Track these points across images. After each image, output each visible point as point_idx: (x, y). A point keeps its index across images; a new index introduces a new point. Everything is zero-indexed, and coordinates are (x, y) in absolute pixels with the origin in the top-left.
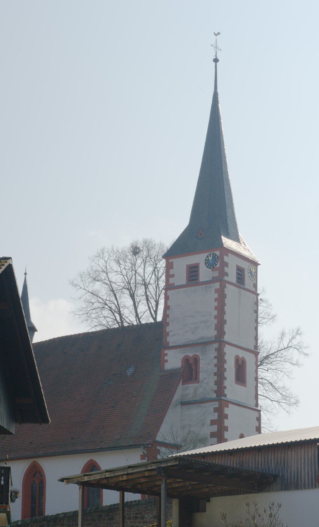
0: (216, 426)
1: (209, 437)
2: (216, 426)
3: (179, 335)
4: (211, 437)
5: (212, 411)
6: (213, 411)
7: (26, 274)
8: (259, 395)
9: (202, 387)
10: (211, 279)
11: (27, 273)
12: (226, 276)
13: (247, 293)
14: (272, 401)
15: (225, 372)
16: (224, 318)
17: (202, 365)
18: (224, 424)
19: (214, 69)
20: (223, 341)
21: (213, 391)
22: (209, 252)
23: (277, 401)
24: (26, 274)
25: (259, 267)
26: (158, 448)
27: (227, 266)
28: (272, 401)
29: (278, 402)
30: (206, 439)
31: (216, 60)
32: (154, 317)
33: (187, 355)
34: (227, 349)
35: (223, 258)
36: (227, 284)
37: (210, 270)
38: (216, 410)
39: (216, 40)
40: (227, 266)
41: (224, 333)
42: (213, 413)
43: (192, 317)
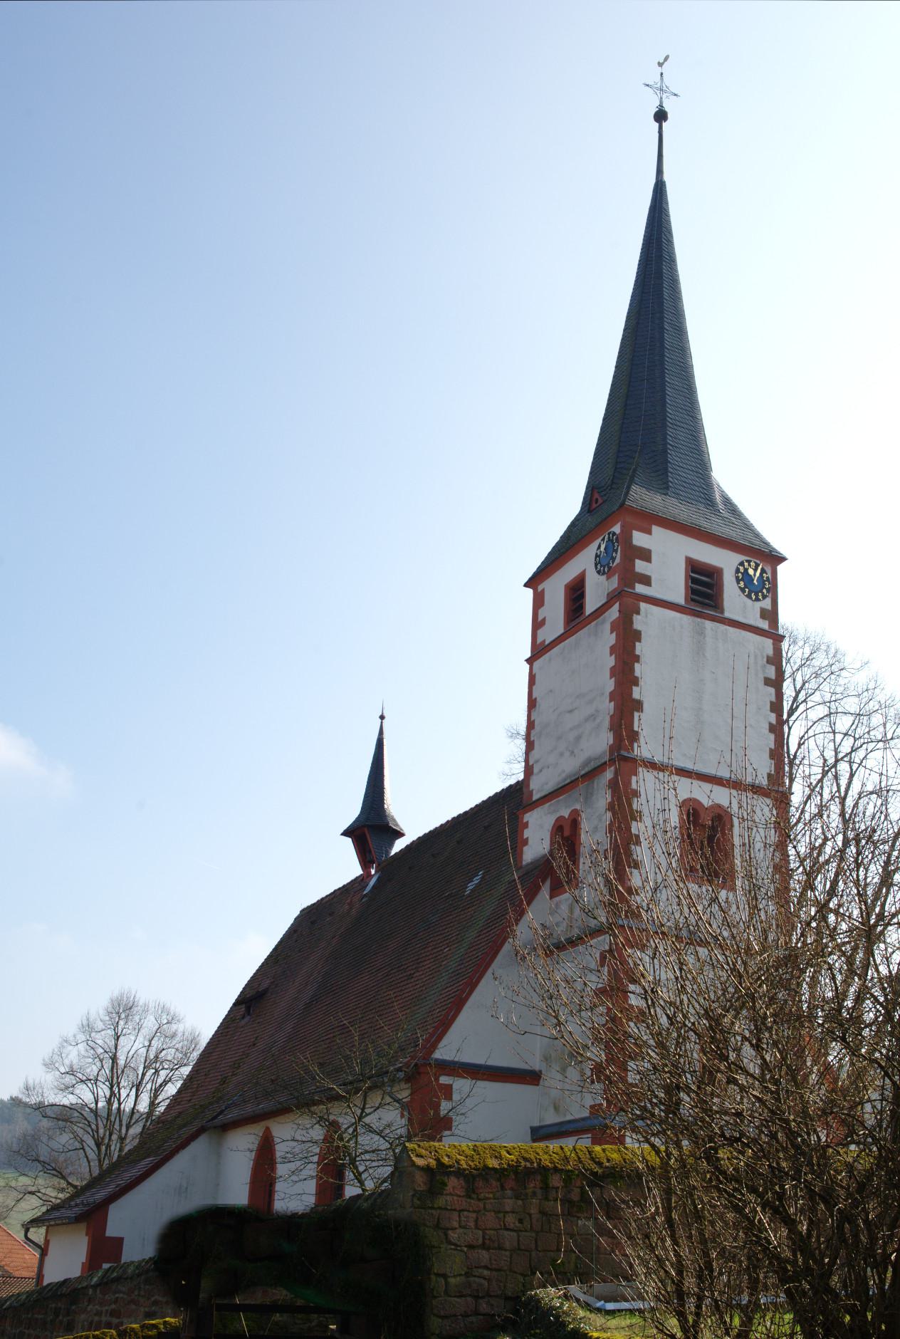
3: (548, 767)
7: (382, 717)
10: (604, 601)
11: (385, 714)
13: (731, 630)
16: (632, 694)
19: (657, 135)
20: (634, 760)
22: (600, 537)
24: (382, 717)
25: (781, 568)
31: (661, 116)
32: (847, 818)
33: (561, 816)
34: (645, 782)
35: (631, 537)
36: (643, 606)
37: (604, 577)
39: (662, 74)
41: (634, 736)
43: (571, 711)
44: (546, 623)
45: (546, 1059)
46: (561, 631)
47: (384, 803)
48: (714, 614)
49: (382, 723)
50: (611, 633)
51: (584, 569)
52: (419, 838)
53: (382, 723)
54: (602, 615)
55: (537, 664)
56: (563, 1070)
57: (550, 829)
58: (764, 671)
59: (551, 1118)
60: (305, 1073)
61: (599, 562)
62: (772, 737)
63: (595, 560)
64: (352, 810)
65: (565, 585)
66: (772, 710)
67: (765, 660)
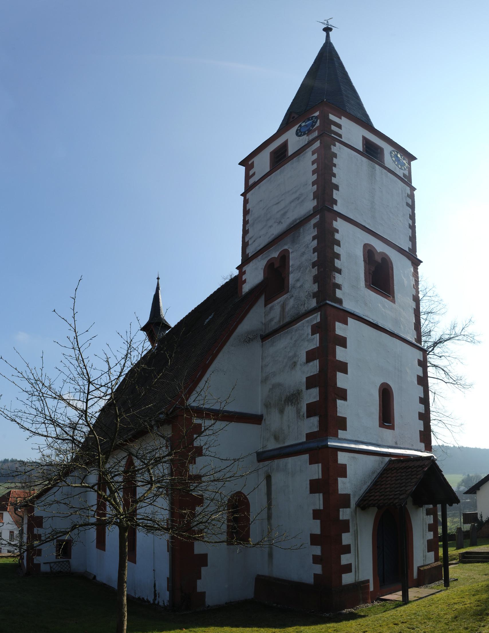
0: (317, 362)
1: (304, 387)
2: (317, 362)
4: (308, 388)
5: (308, 334)
6: (310, 333)
7: (158, 279)
8: (429, 377)
9: (293, 296)
11: (159, 277)
12: (334, 167)
14: (446, 383)
15: (423, 430)
17: (293, 261)
18: (335, 357)
21: (310, 296)
23: (452, 383)
24: (158, 279)
26: (196, 421)
27: (336, 158)
28: (446, 383)
29: (453, 384)
30: (299, 394)
38: (315, 329)
40: (336, 158)
42: (310, 336)
44: (256, 174)
45: (267, 405)
46: (268, 169)
47: (160, 312)
48: (241, 315)
49: (158, 281)
50: (313, 175)
51: (286, 139)
52: (178, 322)
53: (158, 281)
54: (311, 146)
55: (248, 196)
56: (282, 412)
57: (222, 285)
58: (406, 200)
59: (272, 445)
60: (171, 383)
61: (300, 130)
62: (410, 231)
63: (298, 128)
64: (145, 319)
65: (270, 153)
66: (410, 218)
67: (406, 195)
